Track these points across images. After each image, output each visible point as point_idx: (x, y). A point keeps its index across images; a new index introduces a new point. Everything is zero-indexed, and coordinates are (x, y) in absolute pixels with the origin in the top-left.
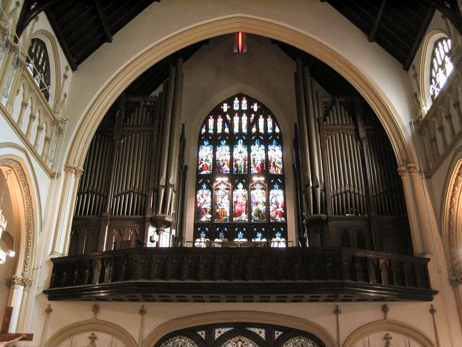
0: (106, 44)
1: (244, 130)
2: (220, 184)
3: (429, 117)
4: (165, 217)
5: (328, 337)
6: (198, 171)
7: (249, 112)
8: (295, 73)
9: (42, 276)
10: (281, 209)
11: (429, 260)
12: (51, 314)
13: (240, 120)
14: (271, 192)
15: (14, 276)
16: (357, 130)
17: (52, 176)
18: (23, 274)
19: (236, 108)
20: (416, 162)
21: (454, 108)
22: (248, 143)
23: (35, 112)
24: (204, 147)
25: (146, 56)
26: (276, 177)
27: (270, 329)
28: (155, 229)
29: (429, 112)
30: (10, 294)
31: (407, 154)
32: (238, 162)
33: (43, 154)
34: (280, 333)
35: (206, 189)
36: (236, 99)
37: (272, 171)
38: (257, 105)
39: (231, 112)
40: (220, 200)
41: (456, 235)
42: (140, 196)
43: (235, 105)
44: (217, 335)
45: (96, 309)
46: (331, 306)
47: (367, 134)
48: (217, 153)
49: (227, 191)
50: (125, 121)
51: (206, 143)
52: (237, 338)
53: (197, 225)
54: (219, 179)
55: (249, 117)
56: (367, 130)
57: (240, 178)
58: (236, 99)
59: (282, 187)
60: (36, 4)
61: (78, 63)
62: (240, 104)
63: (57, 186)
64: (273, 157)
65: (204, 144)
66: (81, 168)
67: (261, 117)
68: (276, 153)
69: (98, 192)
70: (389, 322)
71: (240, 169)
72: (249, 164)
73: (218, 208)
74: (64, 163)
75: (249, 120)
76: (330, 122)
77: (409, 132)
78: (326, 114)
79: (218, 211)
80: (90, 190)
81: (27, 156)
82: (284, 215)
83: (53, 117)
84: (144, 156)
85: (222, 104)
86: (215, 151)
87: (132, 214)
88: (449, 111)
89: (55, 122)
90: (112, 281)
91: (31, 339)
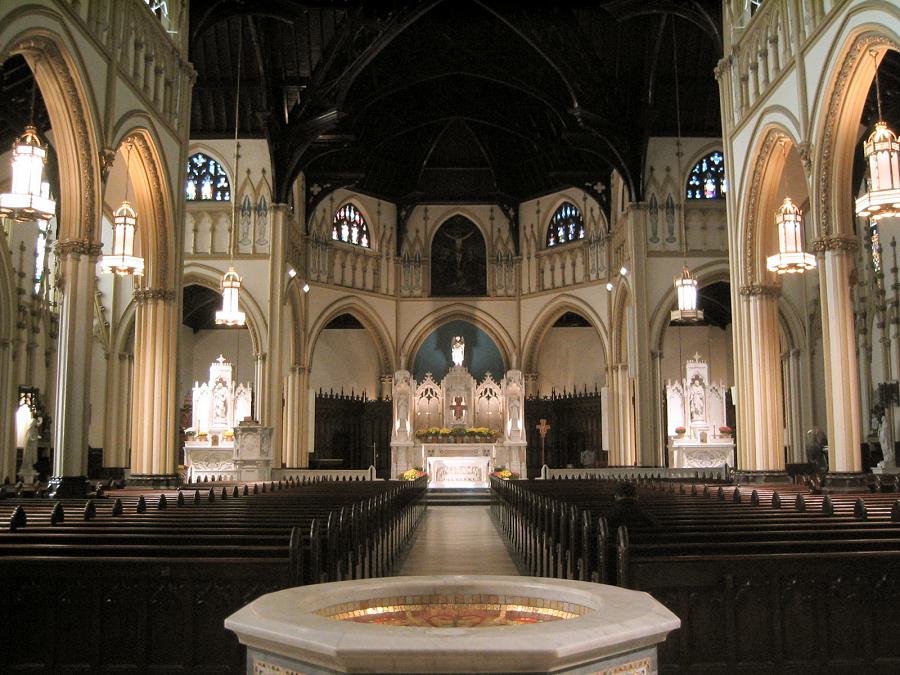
33: (165, 111)
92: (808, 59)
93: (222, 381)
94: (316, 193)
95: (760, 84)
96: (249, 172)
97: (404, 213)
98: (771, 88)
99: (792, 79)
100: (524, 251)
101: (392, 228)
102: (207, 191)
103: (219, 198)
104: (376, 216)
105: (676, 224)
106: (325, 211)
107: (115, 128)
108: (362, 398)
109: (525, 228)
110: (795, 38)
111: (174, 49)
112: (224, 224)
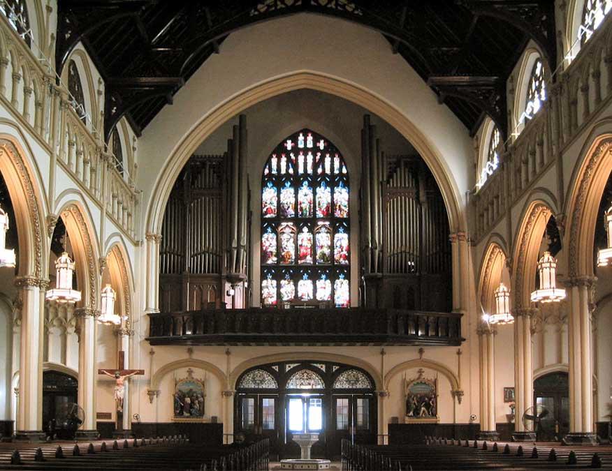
0: (167, 106)
1: (310, 171)
2: (285, 228)
3: (572, 71)
4: (238, 276)
5: (374, 370)
6: (262, 215)
7: (315, 150)
8: (362, 131)
9: (142, 328)
10: (345, 253)
11: (462, 315)
12: (154, 356)
13: (305, 159)
14: (337, 235)
15: (26, 277)
16: (418, 193)
17: (136, 244)
18: (126, 327)
19: (301, 145)
20: (467, 232)
21: (581, 93)
22: (314, 185)
23: (19, 69)
24: (267, 189)
25: (210, 120)
26: (341, 220)
27: (329, 365)
28: (230, 285)
29: (574, 62)
30: (119, 343)
31: (459, 224)
32: (303, 206)
33: (91, 187)
34: (337, 367)
35: (272, 233)
36: (301, 135)
37: (338, 214)
38: (324, 142)
39: (296, 150)
40: (286, 243)
41: (581, 228)
42: (214, 256)
43: (299, 142)
44: (288, 369)
45: (190, 351)
46: (378, 349)
47: (428, 198)
48: (282, 196)
49: (292, 235)
50: (193, 183)
51: (270, 185)
52: (303, 371)
53: (263, 268)
54: (284, 224)
55: (315, 155)
56: (427, 193)
57: (305, 221)
58: (301, 135)
59: (347, 230)
60: (70, 32)
61: (143, 126)
62: (305, 141)
63: (142, 252)
64: (339, 200)
65: (267, 186)
66: (160, 235)
67: (328, 156)
68: (342, 196)
69: (175, 252)
70: (422, 361)
71: (305, 212)
72: (315, 207)
73: (284, 251)
74: (145, 231)
75: (314, 159)
76: (393, 185)
77: (464, 202)
78: (390, 176)
79: (283, 254)
80: (168, 249)
81: (122, 239)
82: (348, 258)
83: (95, 144)
84: (215, 217)
85: (285, 141)
86: (279, 193)
87: (209, 272)
88: (587, 83)
89: (132, 197)
90: (204, 333)
91: (143, 374)
92: (565, 156)
95: (537, 165)
98: (537, 176)
99: (553, 170)
107: (56, 202)
110: (555, 142)
111: (45, 75)
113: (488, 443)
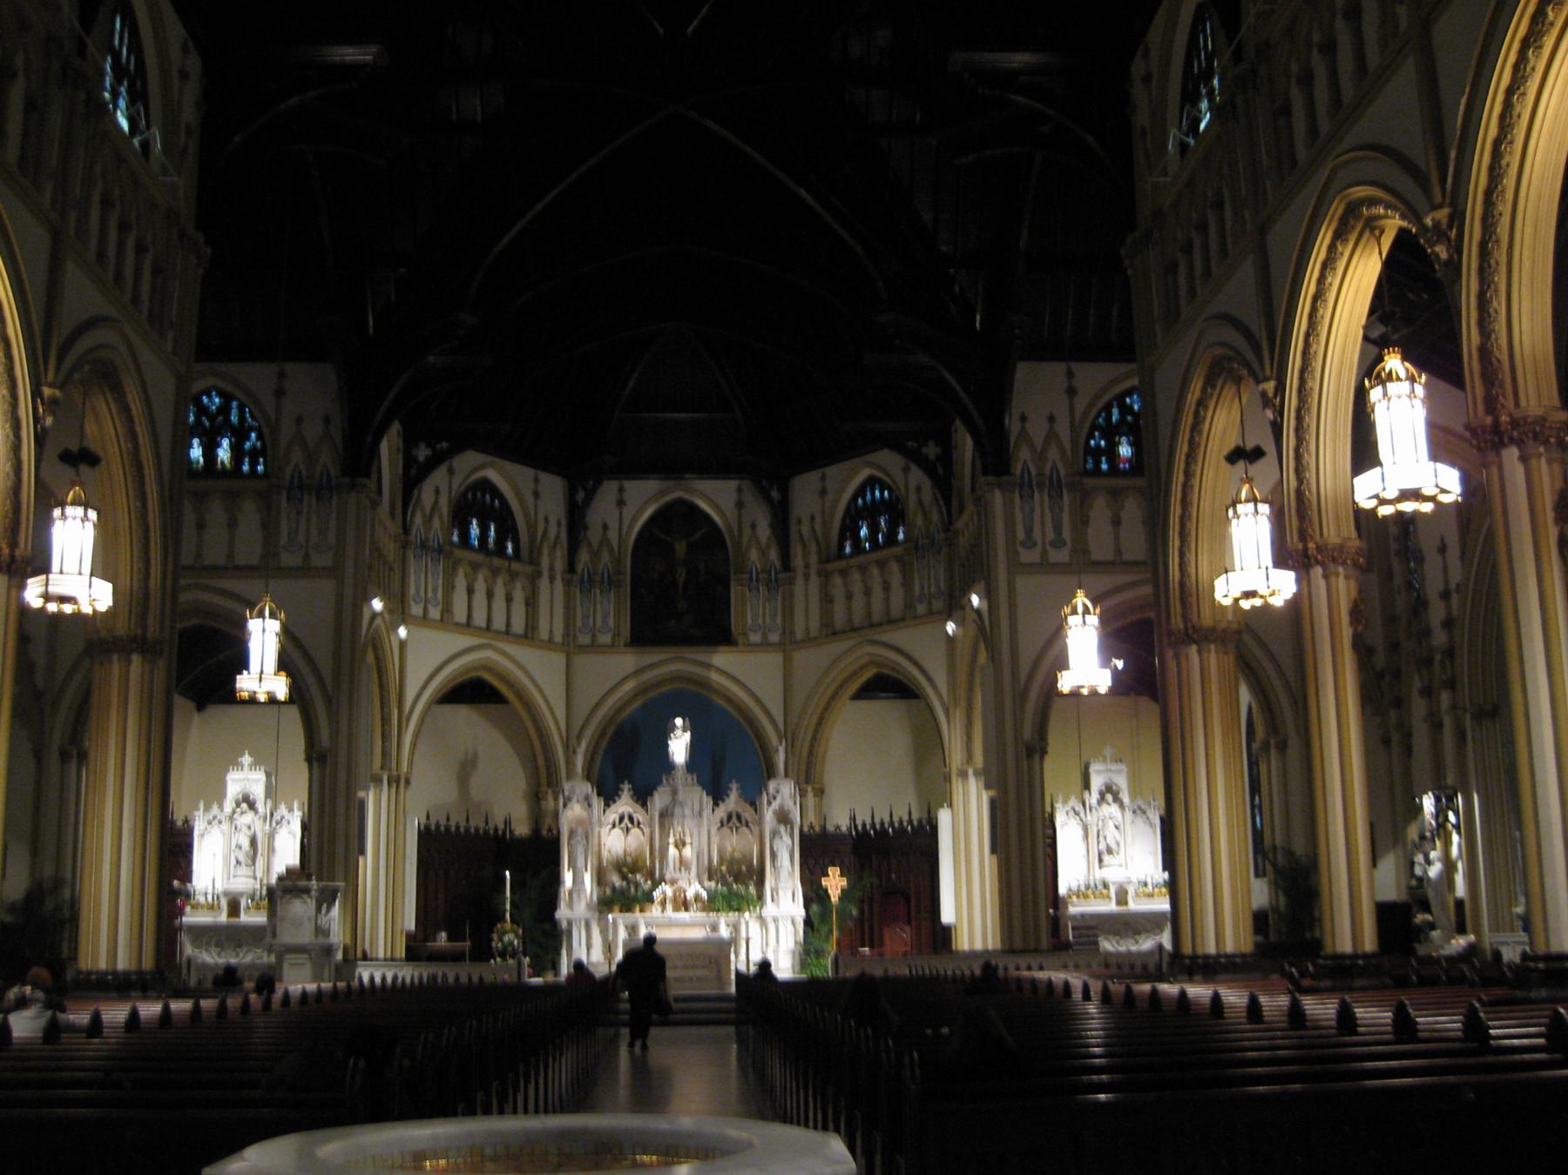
93: (248, 801)
94: (421, 458)
96: (299, 420)
97: (580, 495)
100: (798, 562)
101: (559, 523)
102: (224, 454)
103: (246, 468)
104: (530, 500)
105: (1037, 519)
106: (437, 492)
108: (504, 833)
109: (799, 522)
112: (250, 513)
113: (1311, 1005)
